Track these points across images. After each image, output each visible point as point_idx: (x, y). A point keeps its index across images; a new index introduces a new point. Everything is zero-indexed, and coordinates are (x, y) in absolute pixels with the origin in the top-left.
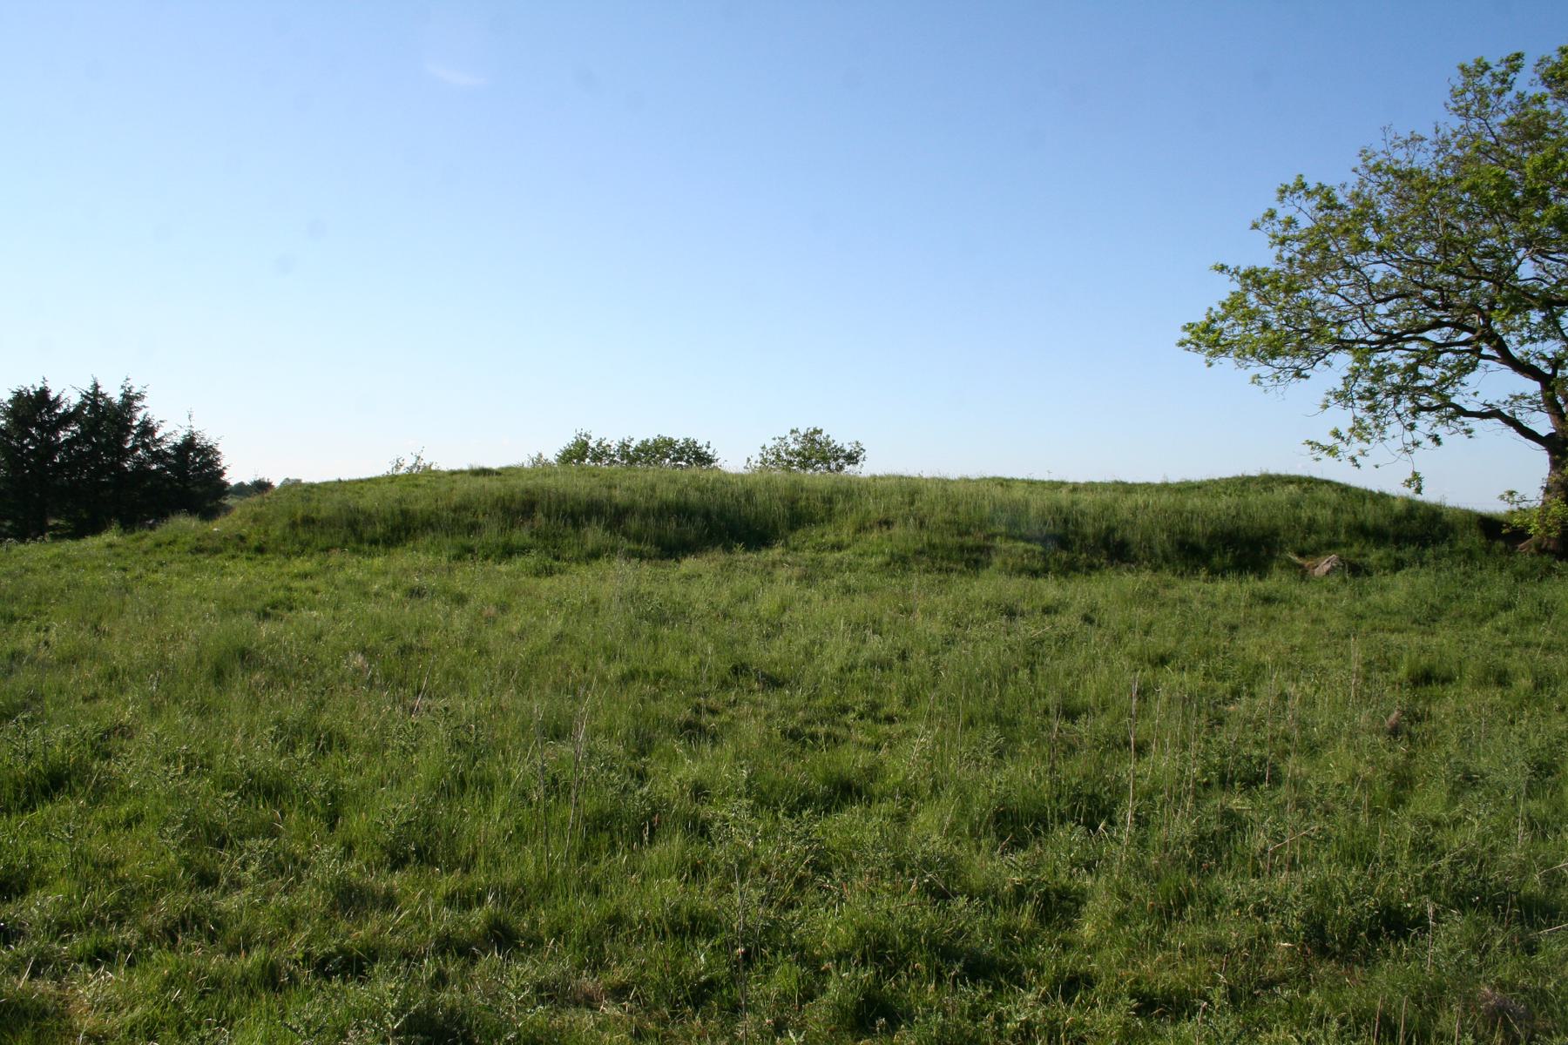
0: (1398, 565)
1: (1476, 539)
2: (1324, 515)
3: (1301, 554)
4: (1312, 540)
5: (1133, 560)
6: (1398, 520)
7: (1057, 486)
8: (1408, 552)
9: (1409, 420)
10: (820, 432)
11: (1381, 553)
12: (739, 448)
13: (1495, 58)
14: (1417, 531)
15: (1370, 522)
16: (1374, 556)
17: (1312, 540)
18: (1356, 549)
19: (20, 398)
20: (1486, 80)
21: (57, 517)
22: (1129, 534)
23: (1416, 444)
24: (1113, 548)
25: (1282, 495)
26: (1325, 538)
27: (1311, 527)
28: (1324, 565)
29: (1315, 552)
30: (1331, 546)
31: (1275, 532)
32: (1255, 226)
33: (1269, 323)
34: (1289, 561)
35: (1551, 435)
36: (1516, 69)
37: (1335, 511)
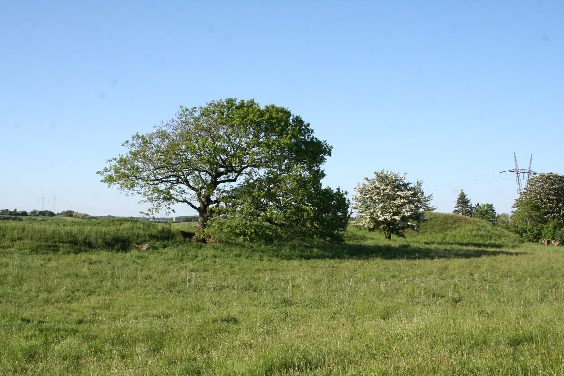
0: (165, 247)
2: (141, 232)
3: (137, 244)
4: (140, 239)
5: (94, 248)
6: (161, 232)
8: (166, 242)
9: (168, 206)
11: (159, 243)
13: (190, 108)
15: (153, 234)
16: (158, 244)
17: (140, 239)
18: (152, 242)
20: (188, 112)
22: (91, 240)
23: (169, 213)
24: (87, 245)
25: (127, 225)
26: (143, 239)
27: (138, 236)
28: (145, 246)
30: (145, 241)
31: (129, 238)
32: (123, 145)
33: (124, 173)
34: (135, 246)
35: (199, 208)
36: (195, 111)
37: (144, 230)
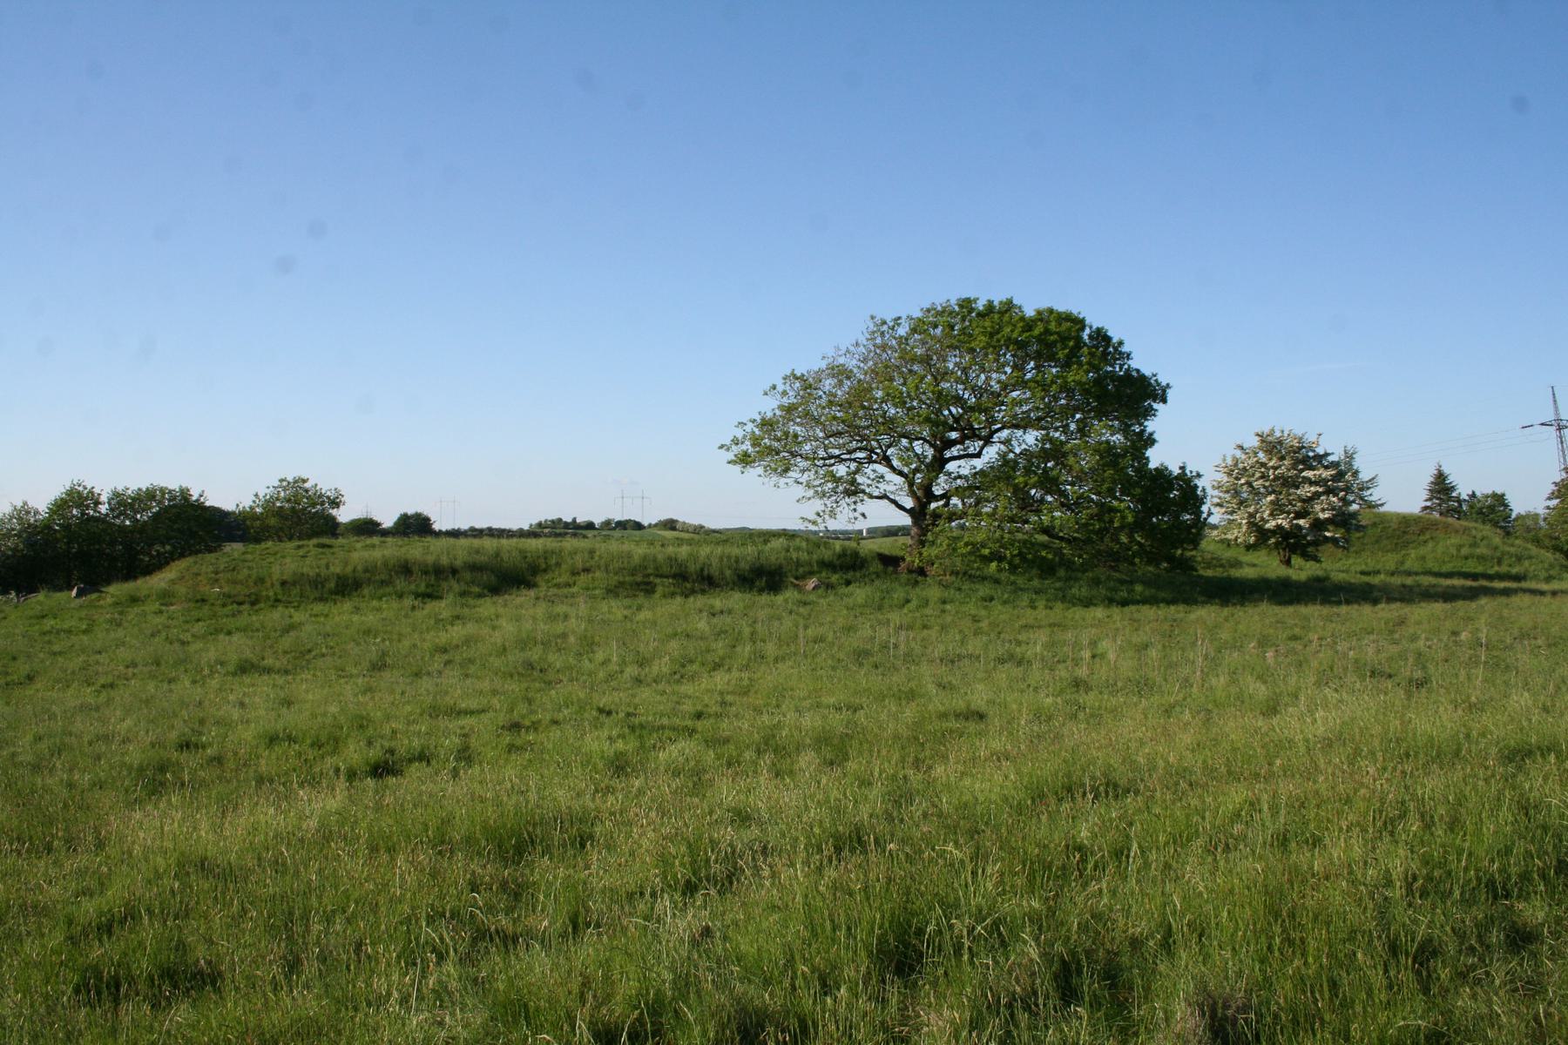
0: (848, 583)
1: (877, 566)
2: (804, 556)
5: (718, 586)
6: (840, 556)
7: (748, 535)
8: (850, 575)
10: (304, 481)
12: (231, 488)
14: (845, 563)
16: (834, 578)
19: (1494, 495)
20: (885, 328)
21: (1146, 537)
25: (777, 544)
27: (798, 564)
28: (811, 583)
29: (803, 577)
30: (811, 573)
31: (781, 567)
33: (769, 447)
